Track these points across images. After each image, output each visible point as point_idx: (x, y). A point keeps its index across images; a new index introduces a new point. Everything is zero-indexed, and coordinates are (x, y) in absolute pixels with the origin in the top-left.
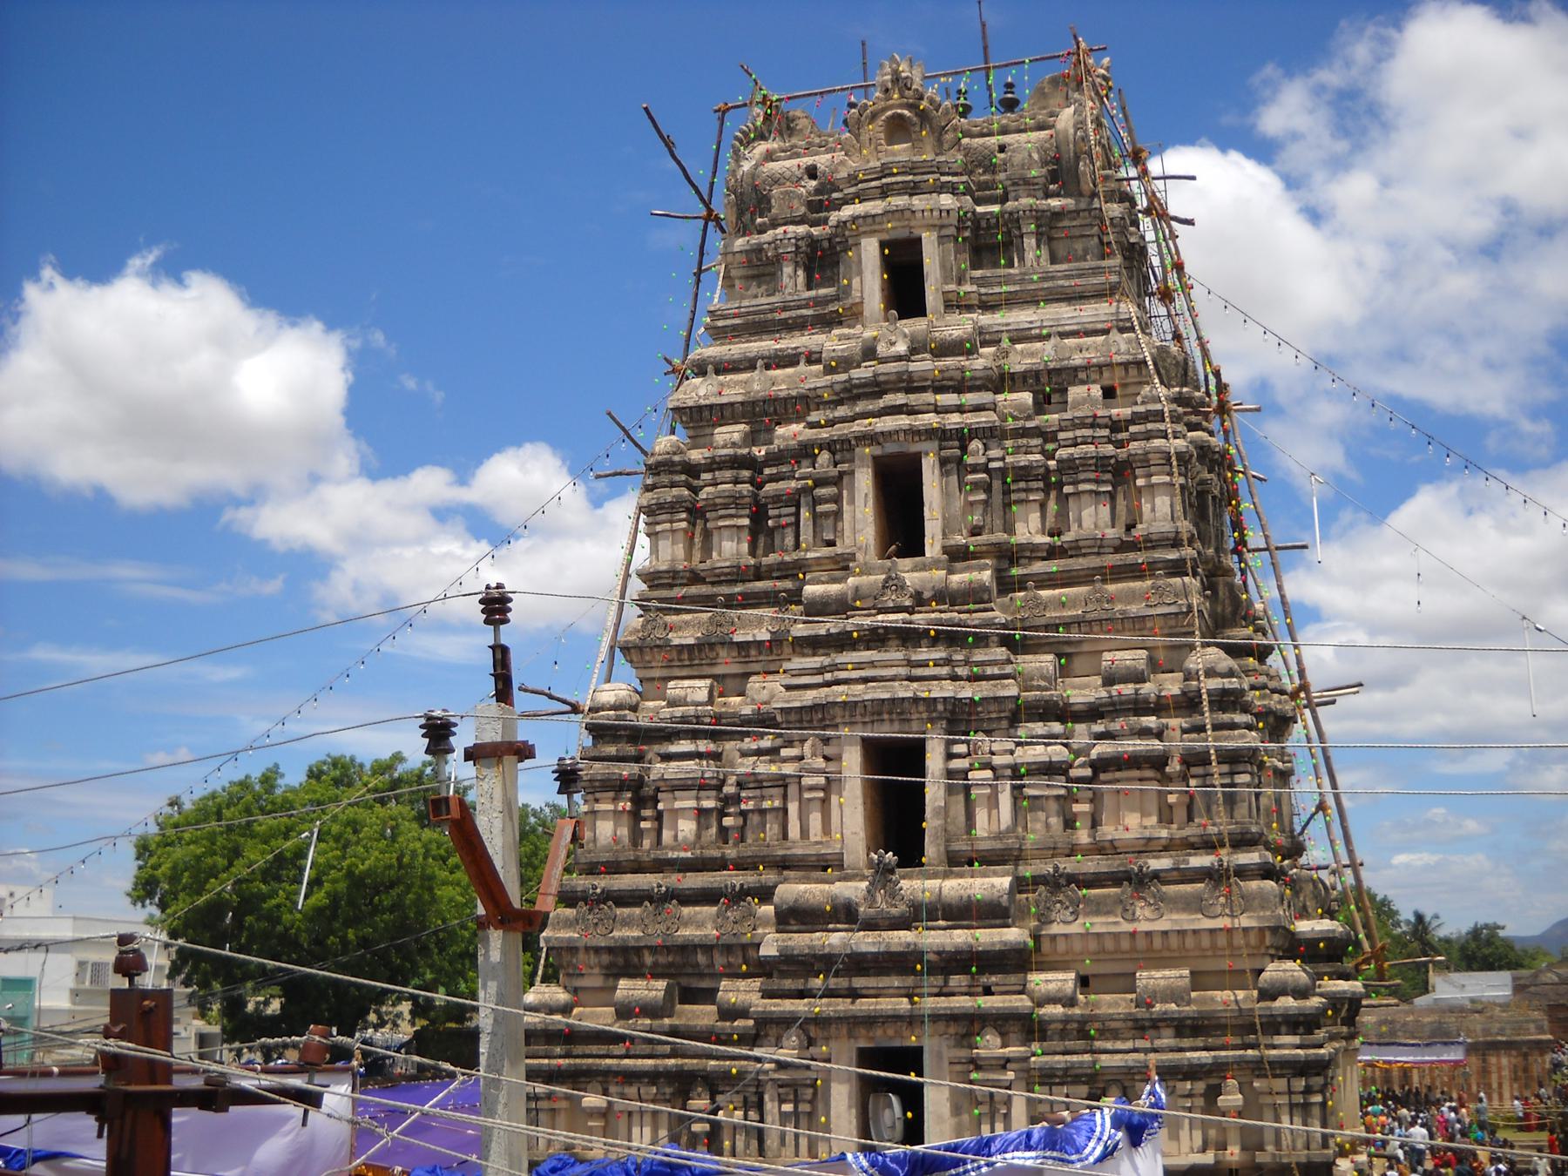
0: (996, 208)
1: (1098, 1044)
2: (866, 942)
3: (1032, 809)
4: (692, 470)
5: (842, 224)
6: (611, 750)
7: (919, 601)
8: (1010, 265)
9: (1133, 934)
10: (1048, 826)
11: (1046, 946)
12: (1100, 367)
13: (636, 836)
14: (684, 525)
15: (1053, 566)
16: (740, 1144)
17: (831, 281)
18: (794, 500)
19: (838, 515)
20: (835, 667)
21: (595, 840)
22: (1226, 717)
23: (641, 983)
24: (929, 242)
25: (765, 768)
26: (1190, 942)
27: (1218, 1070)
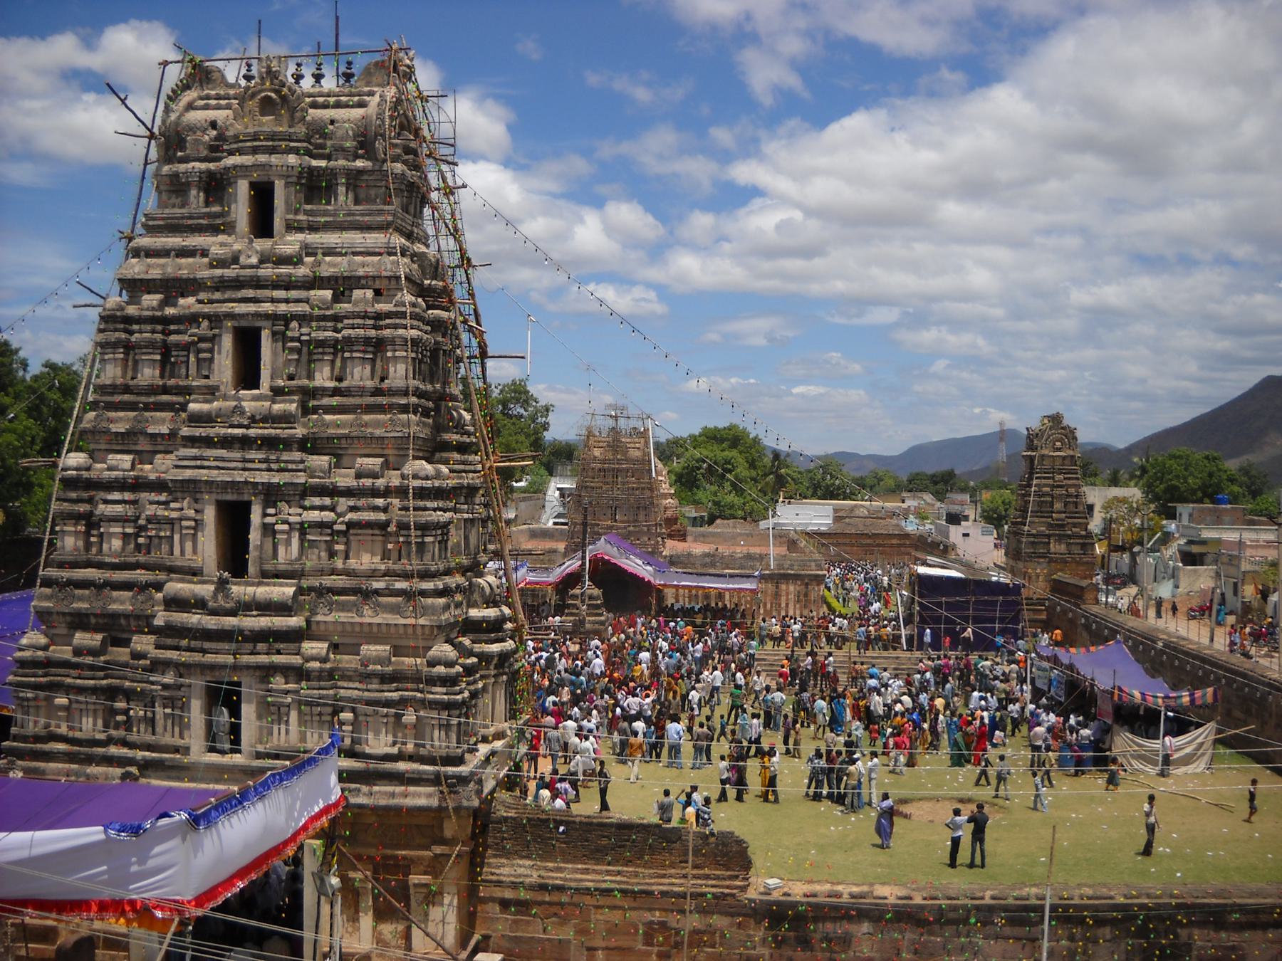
0: (323, 163)
1: (340, 683)
2: (211, 622)
3: (310, 547)
4: (128, 320)
5: (227, 169)
6: (73, 495)
7: (253, 419)
8: (328, 203)
9: (361, 624)
10: (319, 557)
11: (314, 627)
12: (374, 277)
13: (88, 545)
14: (121, 356)
15: (334, 401)
16: (142, 729)
17: (220, 201)
18: (186, 347)
19: (211, 360)
20: (202, 458)
21: (63, 547)
22: (421, 504)
23: (88, 635)
24: (279, 186)
25: (161, 512)
26: (393, 630)
27: (403, 703)
